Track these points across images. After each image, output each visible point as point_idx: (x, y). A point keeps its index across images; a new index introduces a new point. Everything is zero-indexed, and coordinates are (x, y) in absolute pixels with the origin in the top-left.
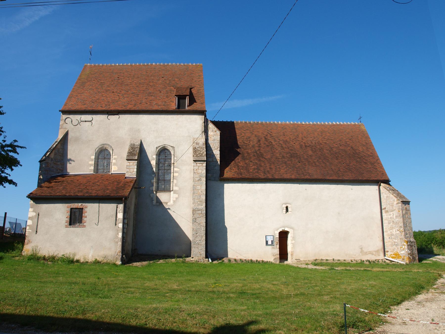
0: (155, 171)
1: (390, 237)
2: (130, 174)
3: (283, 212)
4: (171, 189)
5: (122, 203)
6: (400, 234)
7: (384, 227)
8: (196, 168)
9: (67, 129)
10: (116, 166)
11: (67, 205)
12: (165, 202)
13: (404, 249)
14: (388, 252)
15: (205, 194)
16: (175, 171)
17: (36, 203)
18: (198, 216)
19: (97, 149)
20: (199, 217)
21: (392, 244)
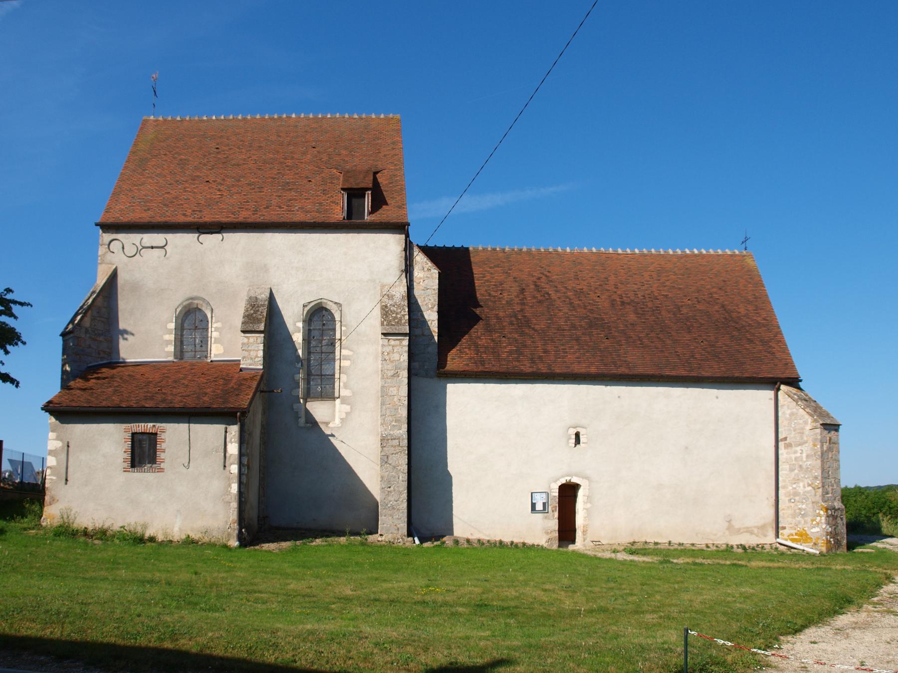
1: (791, 499)
2: (249, 361)
3: (568, 443)
4: (337, 395)
5: (236, 424)
6: (813, 491)
9: (113, 264)
10: (219, 345)
11: (124, 426)
12: (324, 421)
13: (818, 523)
14: (784, 528)
16: (343, 356)
17: (62, 422)
18: (392, 450)
20: (395, 452)
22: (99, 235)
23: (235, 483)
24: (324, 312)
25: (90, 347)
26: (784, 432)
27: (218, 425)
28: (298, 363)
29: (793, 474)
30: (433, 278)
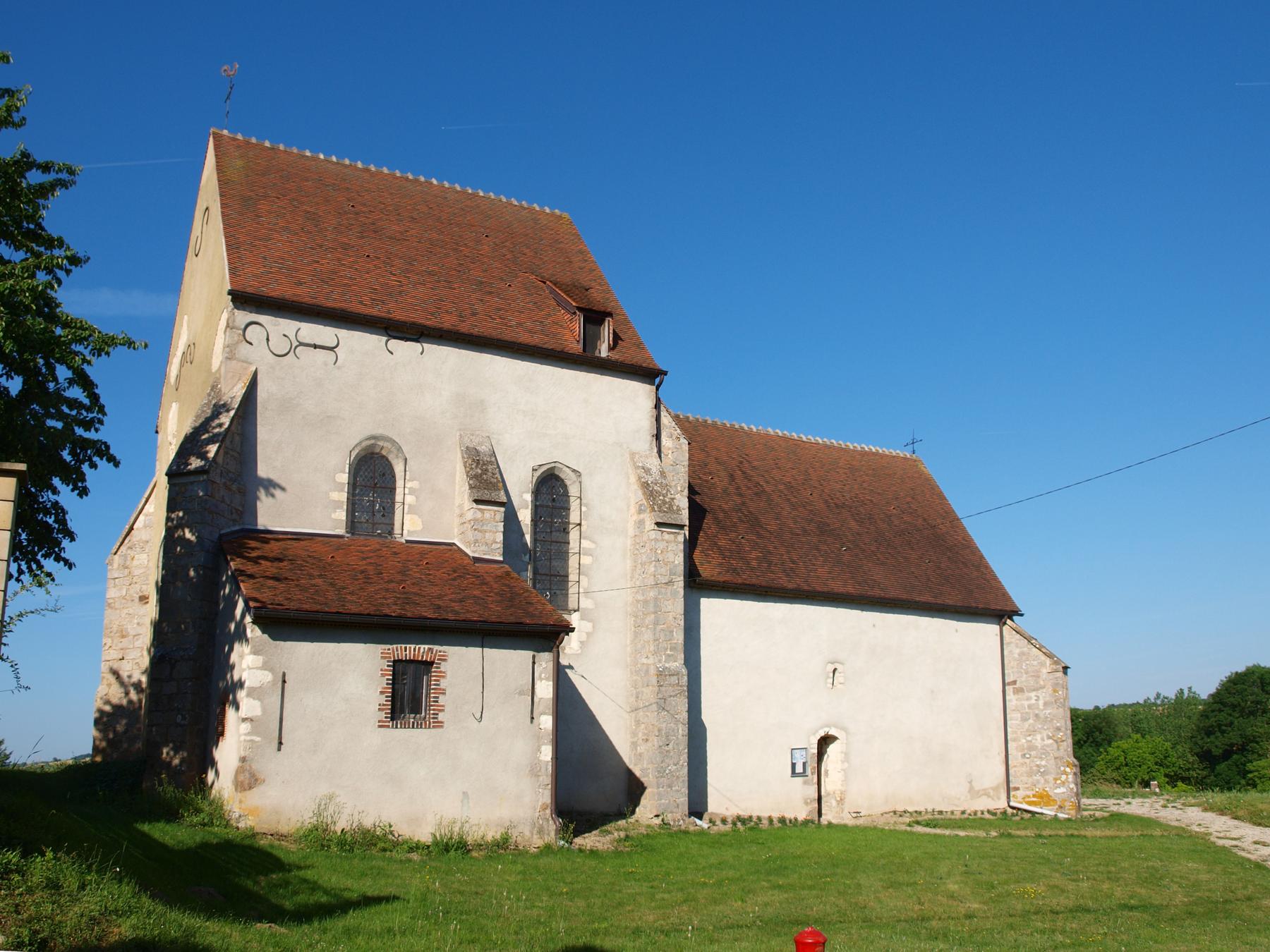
0: (529, 545)
1: (1024, 755)
2: (484, 548)
3: (826, 683)
6: (1055, 746)
7: (1009, 729)
8: (661, 545)
10: (415, 517)
11: (379, 648)
13: (1063, 783)
14: (1017, 789)
15: (683, 627)
16: (583, 548)
17: (275, 637)
19: (356, 451)
21: (1030, 769)
23: (546, 744)
26: (1012, 675)
27: (523, 652)
28: (525, 555)
29: (1026, 725)
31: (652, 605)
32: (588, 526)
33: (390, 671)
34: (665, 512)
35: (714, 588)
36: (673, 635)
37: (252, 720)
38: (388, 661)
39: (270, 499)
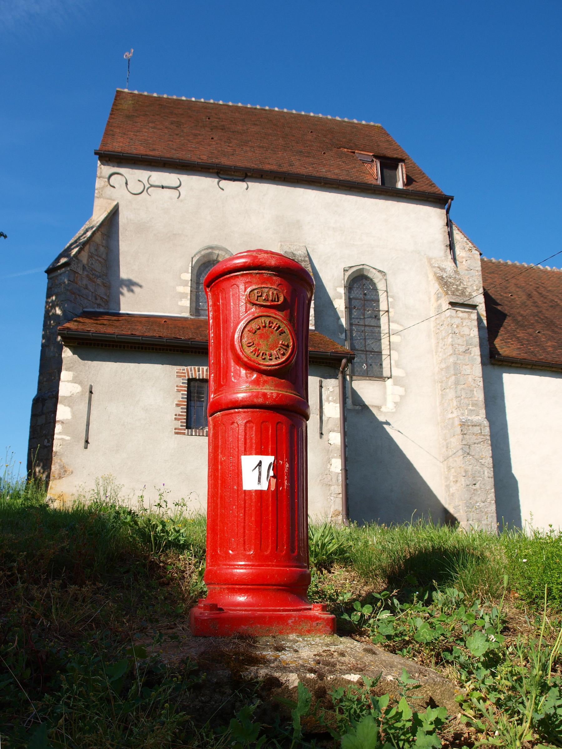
0: (345, 326)
4: (386, 373)
5: (335, 377)
8: (457, 321)
9: (114, 200)
11: (176, 368)
12: (375, 405)
15: (482, 388)
16: (392, 330)
17: (83, 357)
18: (474, 439)
20: (477, 441)
22: (97, 167)
24: (364, 280)
25: (86, 288)
28: (341, 334)
30: (475, 260)
31: (452, 369)
32: (395, 313)
33: (185, 387)
34: (457, 295)
35: (513, 365)
36: (473, 394)
37: (63, 423)
38: (183, 380)
39: (131, 294)
